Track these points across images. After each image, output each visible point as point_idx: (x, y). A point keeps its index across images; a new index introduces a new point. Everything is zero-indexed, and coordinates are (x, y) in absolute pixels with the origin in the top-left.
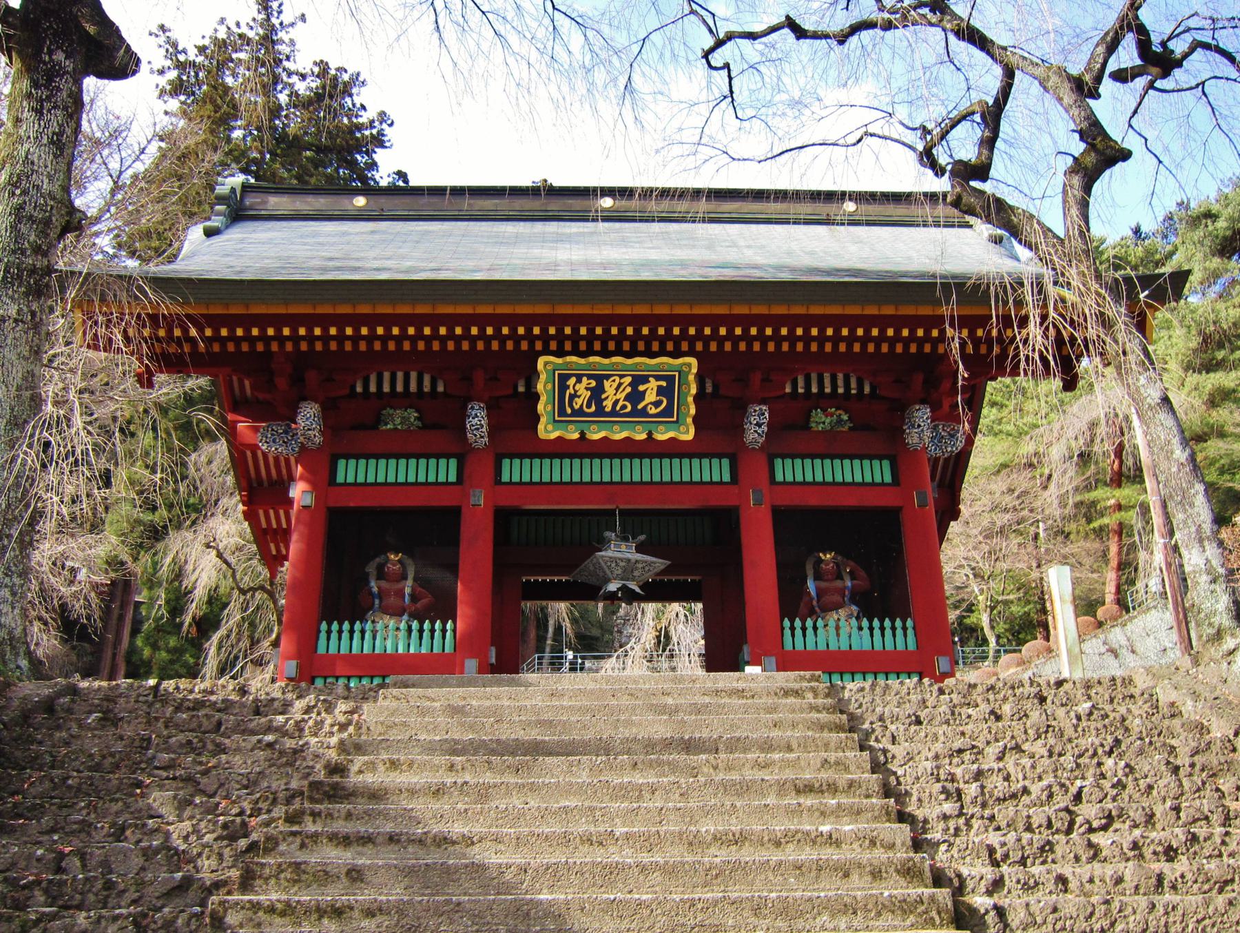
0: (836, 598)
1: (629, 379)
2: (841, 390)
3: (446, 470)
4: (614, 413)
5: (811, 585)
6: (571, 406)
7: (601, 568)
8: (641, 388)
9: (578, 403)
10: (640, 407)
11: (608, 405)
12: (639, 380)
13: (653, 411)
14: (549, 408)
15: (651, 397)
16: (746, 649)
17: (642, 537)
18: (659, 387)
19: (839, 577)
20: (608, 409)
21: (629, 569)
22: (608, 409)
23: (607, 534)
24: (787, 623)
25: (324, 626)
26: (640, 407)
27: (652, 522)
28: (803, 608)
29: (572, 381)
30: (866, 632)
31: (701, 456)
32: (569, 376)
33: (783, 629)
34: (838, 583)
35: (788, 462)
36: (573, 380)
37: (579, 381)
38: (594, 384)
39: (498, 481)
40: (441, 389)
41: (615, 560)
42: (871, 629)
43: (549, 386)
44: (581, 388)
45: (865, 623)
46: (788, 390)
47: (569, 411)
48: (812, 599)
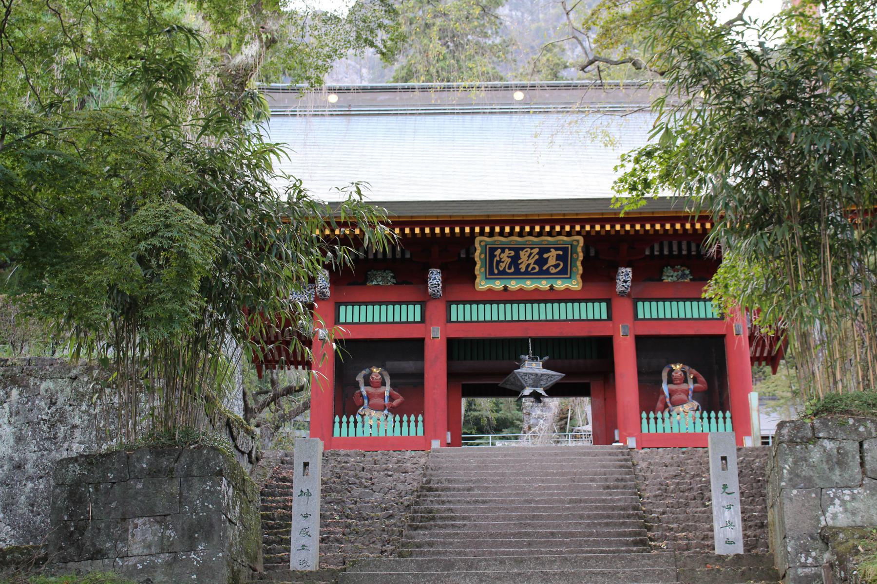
0: (683, 396)
1: (536, 250)
2: (684, 253)
3: (413, 313)
4: (527, 273)
5: (665, 387)
6: (497, 268)
7: (519, 380)
8: (545, 256)
9: (502, 266)
10: (544, 268)
11: (523, 267)
12: (544, 250)
13: (554, 271)
14: (483, 270)
15: (552, 261)
16: (617, 432)
17: (546, 358)
18: (558, 255)
19: (686, 381)
20: (523, 270)
21: (537, 379)
22: (523, 270)
23: (523, 357)
24: (644, 415)
25: (337, 419)
26: (544, 268)
27: (551, 347)
28: (659, 405)
29: (498, 252)
30: (706, 420)
31: (587, 301)
32: (497, 249)
33: (641, 419)
34: (684, 386)
35: (647, 304)
36: (499, 251)
37: (503, 251)
38: (513, 253)
39: (449, 320)
40: (408, 256)
41: (525, 374)
42: (709, 418)
43: (483, 256)
44: (504, 256)
45: (705, 414)
46: (647, 253)
47: (496, 271)
48: (665, 397)
